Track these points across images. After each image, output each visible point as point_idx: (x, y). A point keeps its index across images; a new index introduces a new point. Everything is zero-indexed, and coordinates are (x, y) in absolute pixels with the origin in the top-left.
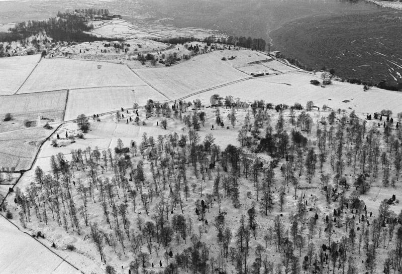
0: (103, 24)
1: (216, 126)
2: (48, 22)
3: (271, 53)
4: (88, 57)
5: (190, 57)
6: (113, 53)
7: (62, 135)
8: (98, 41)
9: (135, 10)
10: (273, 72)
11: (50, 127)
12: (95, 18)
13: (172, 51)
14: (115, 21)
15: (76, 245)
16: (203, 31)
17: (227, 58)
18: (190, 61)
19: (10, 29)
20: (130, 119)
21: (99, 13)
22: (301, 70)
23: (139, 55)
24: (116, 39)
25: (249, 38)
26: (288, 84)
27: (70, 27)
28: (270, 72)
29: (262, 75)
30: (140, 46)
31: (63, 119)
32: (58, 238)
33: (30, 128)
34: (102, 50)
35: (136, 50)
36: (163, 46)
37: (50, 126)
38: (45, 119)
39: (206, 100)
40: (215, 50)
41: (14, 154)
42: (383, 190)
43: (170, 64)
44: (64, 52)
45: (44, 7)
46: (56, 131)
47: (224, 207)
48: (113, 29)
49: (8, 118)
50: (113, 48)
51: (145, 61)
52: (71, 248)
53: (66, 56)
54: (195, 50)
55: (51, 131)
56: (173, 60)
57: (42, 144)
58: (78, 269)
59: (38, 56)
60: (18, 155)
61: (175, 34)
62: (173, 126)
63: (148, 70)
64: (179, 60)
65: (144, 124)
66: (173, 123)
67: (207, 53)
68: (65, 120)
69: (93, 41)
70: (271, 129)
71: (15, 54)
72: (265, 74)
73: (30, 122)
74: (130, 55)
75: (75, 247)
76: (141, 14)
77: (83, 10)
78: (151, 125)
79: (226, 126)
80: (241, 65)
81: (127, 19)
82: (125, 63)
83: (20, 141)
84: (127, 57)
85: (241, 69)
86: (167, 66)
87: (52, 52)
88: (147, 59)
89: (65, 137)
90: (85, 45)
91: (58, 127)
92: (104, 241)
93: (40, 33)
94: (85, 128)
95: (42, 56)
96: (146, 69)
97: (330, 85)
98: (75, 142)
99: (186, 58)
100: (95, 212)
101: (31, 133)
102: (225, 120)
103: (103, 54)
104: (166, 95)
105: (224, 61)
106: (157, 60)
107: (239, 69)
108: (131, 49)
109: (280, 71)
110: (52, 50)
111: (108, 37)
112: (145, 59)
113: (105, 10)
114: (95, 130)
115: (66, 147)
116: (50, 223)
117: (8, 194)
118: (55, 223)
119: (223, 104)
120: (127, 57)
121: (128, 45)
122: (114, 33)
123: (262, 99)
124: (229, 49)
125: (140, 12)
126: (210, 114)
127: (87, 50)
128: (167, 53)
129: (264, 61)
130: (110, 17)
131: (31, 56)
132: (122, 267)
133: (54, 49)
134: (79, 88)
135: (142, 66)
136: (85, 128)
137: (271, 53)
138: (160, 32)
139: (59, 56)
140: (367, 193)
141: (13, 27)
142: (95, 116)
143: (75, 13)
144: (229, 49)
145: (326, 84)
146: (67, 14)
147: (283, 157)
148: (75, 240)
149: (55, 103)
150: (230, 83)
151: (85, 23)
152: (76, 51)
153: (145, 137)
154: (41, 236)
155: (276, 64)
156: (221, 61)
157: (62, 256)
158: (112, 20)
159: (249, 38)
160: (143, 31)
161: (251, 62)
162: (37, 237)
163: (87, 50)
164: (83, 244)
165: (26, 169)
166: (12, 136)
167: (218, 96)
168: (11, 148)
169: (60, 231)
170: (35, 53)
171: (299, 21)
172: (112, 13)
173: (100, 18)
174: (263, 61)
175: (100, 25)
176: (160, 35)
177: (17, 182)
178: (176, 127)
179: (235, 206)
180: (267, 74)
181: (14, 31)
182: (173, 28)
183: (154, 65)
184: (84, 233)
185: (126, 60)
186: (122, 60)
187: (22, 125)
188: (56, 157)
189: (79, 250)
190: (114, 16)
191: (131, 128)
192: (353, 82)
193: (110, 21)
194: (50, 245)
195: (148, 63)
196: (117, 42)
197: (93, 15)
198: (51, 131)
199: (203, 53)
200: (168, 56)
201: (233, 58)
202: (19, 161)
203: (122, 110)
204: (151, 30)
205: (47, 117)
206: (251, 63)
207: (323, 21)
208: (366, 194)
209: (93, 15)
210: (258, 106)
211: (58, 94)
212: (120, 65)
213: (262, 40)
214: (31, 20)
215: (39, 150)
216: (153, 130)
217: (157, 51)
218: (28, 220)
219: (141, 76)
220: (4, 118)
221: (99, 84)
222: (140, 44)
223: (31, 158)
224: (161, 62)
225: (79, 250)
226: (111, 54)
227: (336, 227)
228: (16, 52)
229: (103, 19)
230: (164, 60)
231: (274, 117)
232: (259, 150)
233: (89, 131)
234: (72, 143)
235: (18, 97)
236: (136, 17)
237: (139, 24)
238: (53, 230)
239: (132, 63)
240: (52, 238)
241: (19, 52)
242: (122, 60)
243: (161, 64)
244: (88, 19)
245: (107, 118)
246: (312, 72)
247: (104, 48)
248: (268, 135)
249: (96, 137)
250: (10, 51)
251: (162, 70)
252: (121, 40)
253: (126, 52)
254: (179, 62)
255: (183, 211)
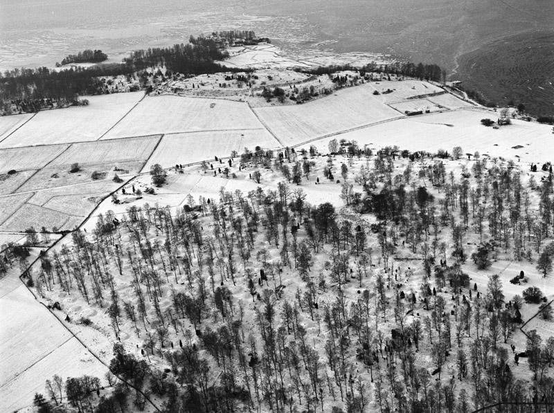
1: (323, 179)
4: (202, 93)
6: (235, 88)
8: (220, 73)
9: (293, 31)
10: (438, 109)
13: (308, 85)
14: (260, 46)
16: (369, 57)
17: (380, 91)
19: (125, 60)
20: (220, 170)
22: (480, 106)
23: (265, 90)
25: (420, 64)
26: (448, 125)
28: (433, 108)
29: (421, 113)
30: (270, 78)
34: (220, 85)
35: (264, 83)
37: (120, 178)
38: (119, 170)
42: (514, 264)
44: (174, 87)
45: (178, 30)
46: (125, 184)
49: (76, 169)
51: (272, 97)
52: (87, 322)
53: (175, 92)
54: (341, 83)
55: (120, 185)
56: (307, 96)
57: (103, 200)
59: (142, 93)
61: (329, 61)
64: (316, 95)
65: (234, 176)
66: (271, 175)
67: (356, 85)
70: (390, 183)
71: (115, 91)
72: (424, 112)
74: (256, 89)
78: (243, 177)
79: (336, 179)
81: (276, 43)
82: (245, 100)
83: (77, 197)
85: (395, 106)
86: (299, 103)
88: (275, 95)
89: (132, 192)
91: (130, 180)
93: (159, 64)
94: (160, 180)
95: (146, 93)
97: (508, 126)
98: (141, 198)
101: (96, 187)
102: (337, 173)
103: (220, 89)
106: (287, 96)
111: (243, 68)
112: (272, 94)
113: (250, 32)
116: (73, 293)
118: (77, 293)
120: (250, 93)
121: (256, 78)
123: (396, 145)
124: (389, 79)
128: (300, 87)
129: (431, 95)
130: (254, 41)
133: (164, 83)
134: (278, 137)
139: (166, 93)
140: (488, 268)
141: (128, 56)
142: (177, 166)
143: (212, 36)
144: (389, 79)
145: (502, 124)
148: (95, 313)
150: (371, 125)
154: (57, 307)
155: (448, 99)
161: (411, 96)
163: (203, 85)
166: (72, 190)
169: (81, 302)
171: (507, 40)
172: (258, 35)
175: (239, 52)
177: (55, 244)
180: (428, 112)
182: (331, 54)
183: (282, 102)
185: (248, 97)
186: (242, 97)
189: (96, 324)
190: (261, 40)
192: (541, 121)
193: (255, 46)
195: (275, 100)
196: (244, 74)
197: (234, 39)
199: (352, 86)
201: (389, 91)
203: (216, 159)
205: (123, 168)
206: (411, 98)
207: (542, 38)
208: (487, 270)
209: (234, 39)
210: (388, 153)
212: (240, 103)
215: (96, 208)
216: (244, 186)
220: (71, 170)
221: (205, 126)
222: (272, 76)
224: (292, 98)
228: (117, 88)
229: (246, 44)
230: (296, 96)
233: (165, 186)
234: (137, 199)
235: (100, 144)
236: (289, 40)
237: (290, 49)
238: (74, 301)
242: (243, 96)
243: (292, 101)
244: (227, 44)
245: (192, 170)
246: (492, 109)
247: (223, 81)
251: (291, 109)
254: (316, 98)
255: (234, 283)
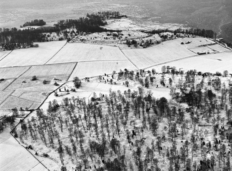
0: (114, 21)
1: (160, 85)
2: (79, 20)
3: (217, 39)
4: (96, 42)
5: (160, 42)
6: (112, 40)
7: (63, 90)
8: (104, 32)
10: (213, 52)
11: (57, 84)
12: (110, 17)
13: (149, 38)
14: (122, 19)
15: (49, 154)
16: (177, 26)
18: (159, 45)
19: (55, 25)
20: (108, 80)
21: (113, 15)
24: (114, 31)
25: (204, 30)
27: (92, 23)
28: (211, 51)
29: (205, 53)
30: (129, 35)
31: (67, 80)
32: (40, 150)
33: (46, 85)
34: (105, 38)
35: (126, 38)
36: (144, 35)
37: (58, 84)
39: (159, 70)
40: (178, 38)
41: (31, 100)
43: (146, 47)
44: (81, 39)
46: (60, 87)
47: (147, 135)
48: (119, 24)
50: (112, 36)
51: (131, 44)
52: (46, 156)
53: (82, 41)
54: (165, 38)
56: (148, 44)
57: (50, 94)
58: (46, 168)
59: (66, 41)
60: (33, 100)
62: (133, 85)
63: (131, 51)
64: (153, 44)
65: (115, 84)
67: (172, 39)
68: (68, 80)
69: (101, 32)
71: (52, 40)
73: (47, 82)
74: (123, 40)
75: (48, 155)
76: (141, 14)
77: (103, 12)
79: (166, 86)
80: (193, 47)
81: (130, 18)
82: (118, 46)
84: (120, 42)
87: (74, 39)
88: (132, 43)
89: (64, 91)
90: (95, 34)
91: (63, 85)
92: (65, 152)
94: (78, 85)
95: (67, 42)
96: (130, 50)
98: (69, 94)
99: (158, 43)
100: (64, 135)
102: (167, 82)
103: (105, 40)
104: (137, 66)
105: (182, 45)
106: (138, 44)
107: (190, 50)
108: (124, 37)
109: (218, 51)
110: (74, 37)
113: (117, 12)
114: (84, 87)
115: (63, 97)
117: (19, 123)
118: (41, 141)
119: (170, 72)
121: (122, 35)
122: (119, 27)
124: (188, 37)
125: (140, 14)
126: (158, 77)
127: (96, 38)
128: (145, 40)
130: (120, 16)
131: (62, 41)
132: (73, 168)
133: (76, 37)
135: (128, 48)
136: (78, 85)
137: (217, 39)
138: (149, 27)
139: (78, 41)
141: (56, 23)
142: (86, 78)
143: (98, 14)
144: (188, 37)
146: (93, 15)
147: (196, 106)
148: (50, 151)
149: (66, 71)
151: (102, 21)
152: (89, 38)
153: (110, 91)
155: (217, 47)
156: (180, 44)
157: (39, 160)
158: (121, 18)
159: (204, 30)
160: (139, 26)
162: (28, 148)
163: (96, 38)
164: (53, 153)
165: (35, 109)
167: (169, 67)
168: (30, 97)
169: (42, 145)
170: (64, 39)
173: (113, 17)
174: (208, 45)
175: (112, 22)
176: (148, 28)
177: (27, 116)
178: (135, 86)
179: (154, 135)
180: (208, 53)
181: (57, 25)
183: (136, 47)
184: (56, 147)
185: (119, 44)
186: (116, 44)
187: (42, 83)
188: (52, 103)
189: (51, 157)
190: (123, 16)
191: (108, 86)
193: (120, 19)
194: (34, 153)
195: (132, 46)
196: (116, 33)
198: (58, 87)
199: (170, 40)
200: (146, 42)
201: (189, 43)
202: (33, 104)
203: (105, 75)
204: (143, 25)
206: (200, 46)
210: (191, 73)
211: (71, 65)
213: (211, 31)
214: (68, 19)
215: (47, 98)
216: (120, 88)
217: (140, 38)
218: (26, 139)
219: (125, 54)
221: (98, 58)
222: (130, 34)
223: (40, 103)
224: (141, 45)
225: (51, 157)
226: (110, 40)
227: (215, 150)
228: (52, 39)
229: (115, 18)
230: (143, 44)
231: (198, 79)
232: (183, 101)
233: (80, 88)
234: (67, 94)
235: (46, 66)
238: (39, 145)
239: (122, 46)
240: (37, 149)
241: (54, 39)
242: (116, 44)
243: (141, 47)
245: (93, 80)
248: (191, 91)
249: (84, 91)
250: (49, 38)
252: (118, 31)
253: (120, 39)
254: (152, 45)
255: (120, 137)
